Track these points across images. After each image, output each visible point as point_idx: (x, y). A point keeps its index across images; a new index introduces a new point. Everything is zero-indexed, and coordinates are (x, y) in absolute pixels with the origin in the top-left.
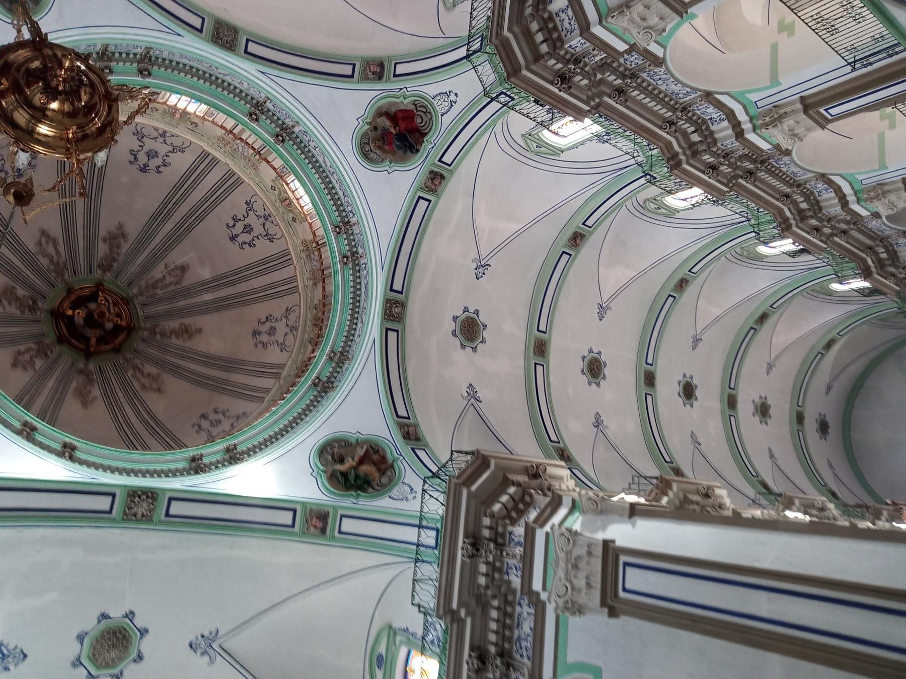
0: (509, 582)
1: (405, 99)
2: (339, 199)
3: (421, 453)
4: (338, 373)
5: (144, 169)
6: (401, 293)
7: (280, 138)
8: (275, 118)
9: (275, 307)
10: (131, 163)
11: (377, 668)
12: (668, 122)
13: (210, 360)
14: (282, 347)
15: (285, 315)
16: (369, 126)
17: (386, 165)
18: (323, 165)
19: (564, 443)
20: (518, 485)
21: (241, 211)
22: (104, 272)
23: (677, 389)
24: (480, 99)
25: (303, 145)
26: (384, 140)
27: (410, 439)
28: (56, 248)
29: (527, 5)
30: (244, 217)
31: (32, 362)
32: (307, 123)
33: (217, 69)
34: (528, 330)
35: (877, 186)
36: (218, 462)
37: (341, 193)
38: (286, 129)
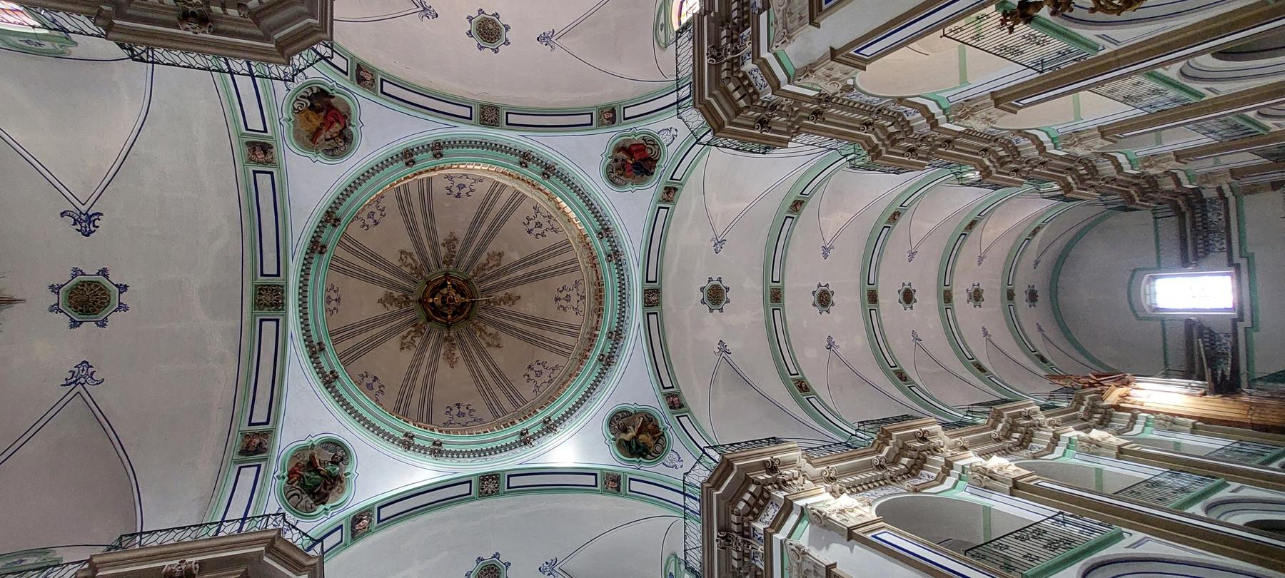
5: (458, 196)
6: (656, 282)
8: (540, 161)
9: (567, 280)
12: (865, 124)
17: (629, 187)
18: (582, 188)
19: (802, 375)
21: (532, 214)
23: (899, 297)
27: (675, 409)
29: (723, 69)
34: (765, 283)
35: (1073, 134)
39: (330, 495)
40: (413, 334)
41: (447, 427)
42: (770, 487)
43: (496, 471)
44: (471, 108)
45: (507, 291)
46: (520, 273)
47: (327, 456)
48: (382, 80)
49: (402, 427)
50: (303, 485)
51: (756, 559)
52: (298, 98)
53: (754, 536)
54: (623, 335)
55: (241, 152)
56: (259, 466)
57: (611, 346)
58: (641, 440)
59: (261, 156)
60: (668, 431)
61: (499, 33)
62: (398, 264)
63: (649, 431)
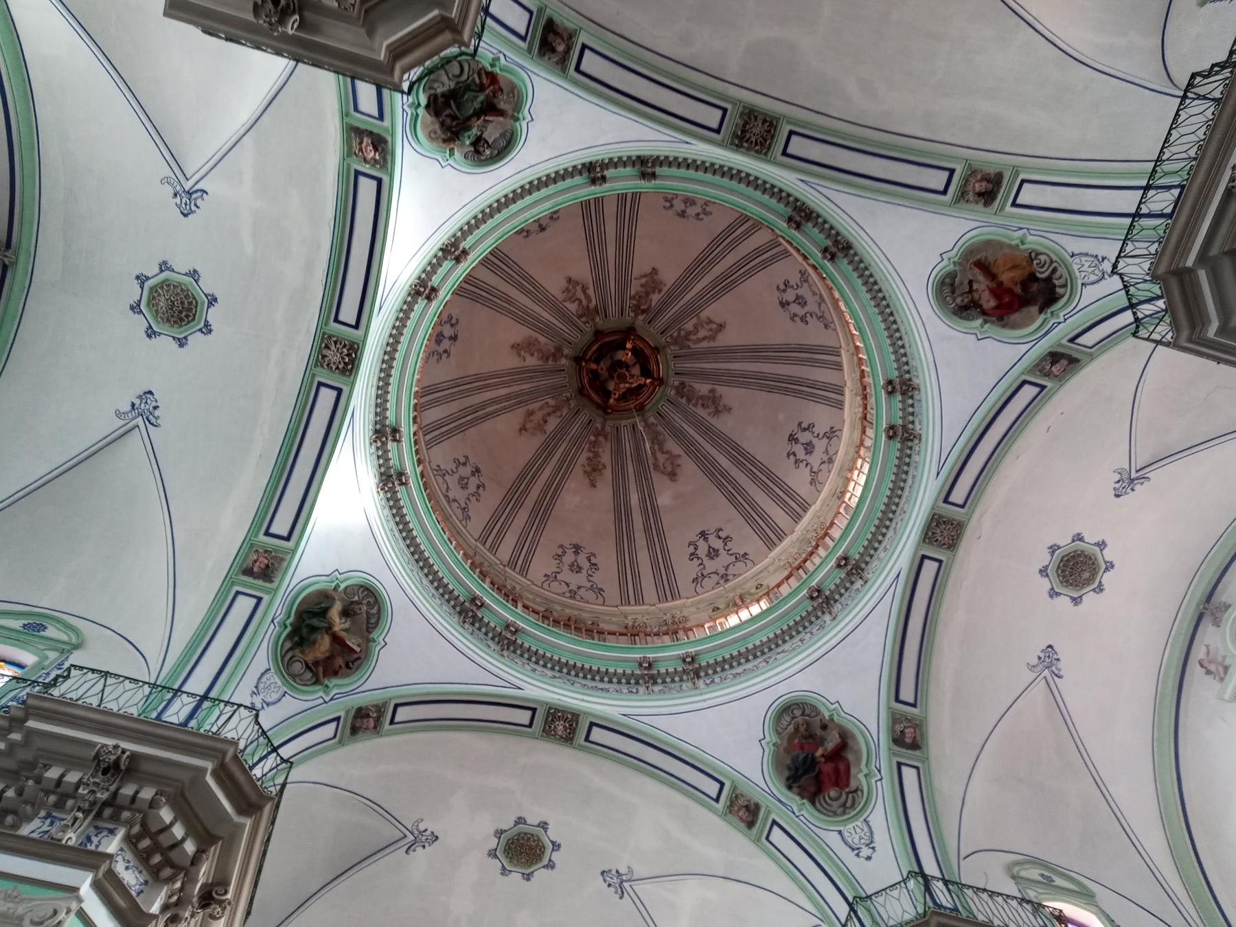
0: (30, 819)
1: (866, 776)
2: (731, 667)
3: (329, 730)
4: (486, 634)
6: (587, 739)
7: (815, 594)
9: (607, 576)
10: (800, 424)
11: (26, 622)
13: (552, 492)
14: (552, 577)
15: (595, 586)
16: (827, 718)
17: (771, 737)
18: (779, 650)
20: (196, 860)
21: (736, 547)
22: (677, 388)
24: (855, 889)
25: (807, 624)
26: (806, 738)
27: (355, 717)
28: (704, 339)
30: (728, 550)
31: (572, 299)
32: (833, 631)
33: (902, 520)
36: (387, 460)
37: (740, 670)
38: (828, 603)
39: (434, 119)
40: (585, 302)
41: (447, 320)
42: (178, 885)
43: (356, 374)
44: (962, 506)
45: (609, 469)
46: (634, 499)
47: (492, 133)
48: (1043, 387)
49: (479, 248)
50: (468, 88)
51: (48, 821)
52: (1054, 265)
53: (97, 828)
54: (506, 653)
55: (991, 163)
56: (523, 39)
57: (492, 625)
58: (322, 638)
59: (979, 187)
60: (321, 694)
61: (1071, 585)
62: (560, 296)
63: (330, 659)
